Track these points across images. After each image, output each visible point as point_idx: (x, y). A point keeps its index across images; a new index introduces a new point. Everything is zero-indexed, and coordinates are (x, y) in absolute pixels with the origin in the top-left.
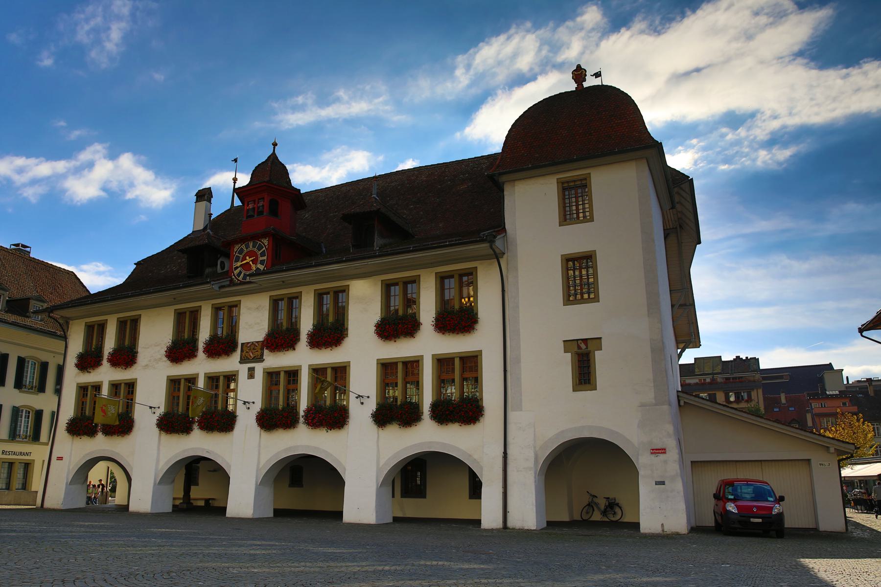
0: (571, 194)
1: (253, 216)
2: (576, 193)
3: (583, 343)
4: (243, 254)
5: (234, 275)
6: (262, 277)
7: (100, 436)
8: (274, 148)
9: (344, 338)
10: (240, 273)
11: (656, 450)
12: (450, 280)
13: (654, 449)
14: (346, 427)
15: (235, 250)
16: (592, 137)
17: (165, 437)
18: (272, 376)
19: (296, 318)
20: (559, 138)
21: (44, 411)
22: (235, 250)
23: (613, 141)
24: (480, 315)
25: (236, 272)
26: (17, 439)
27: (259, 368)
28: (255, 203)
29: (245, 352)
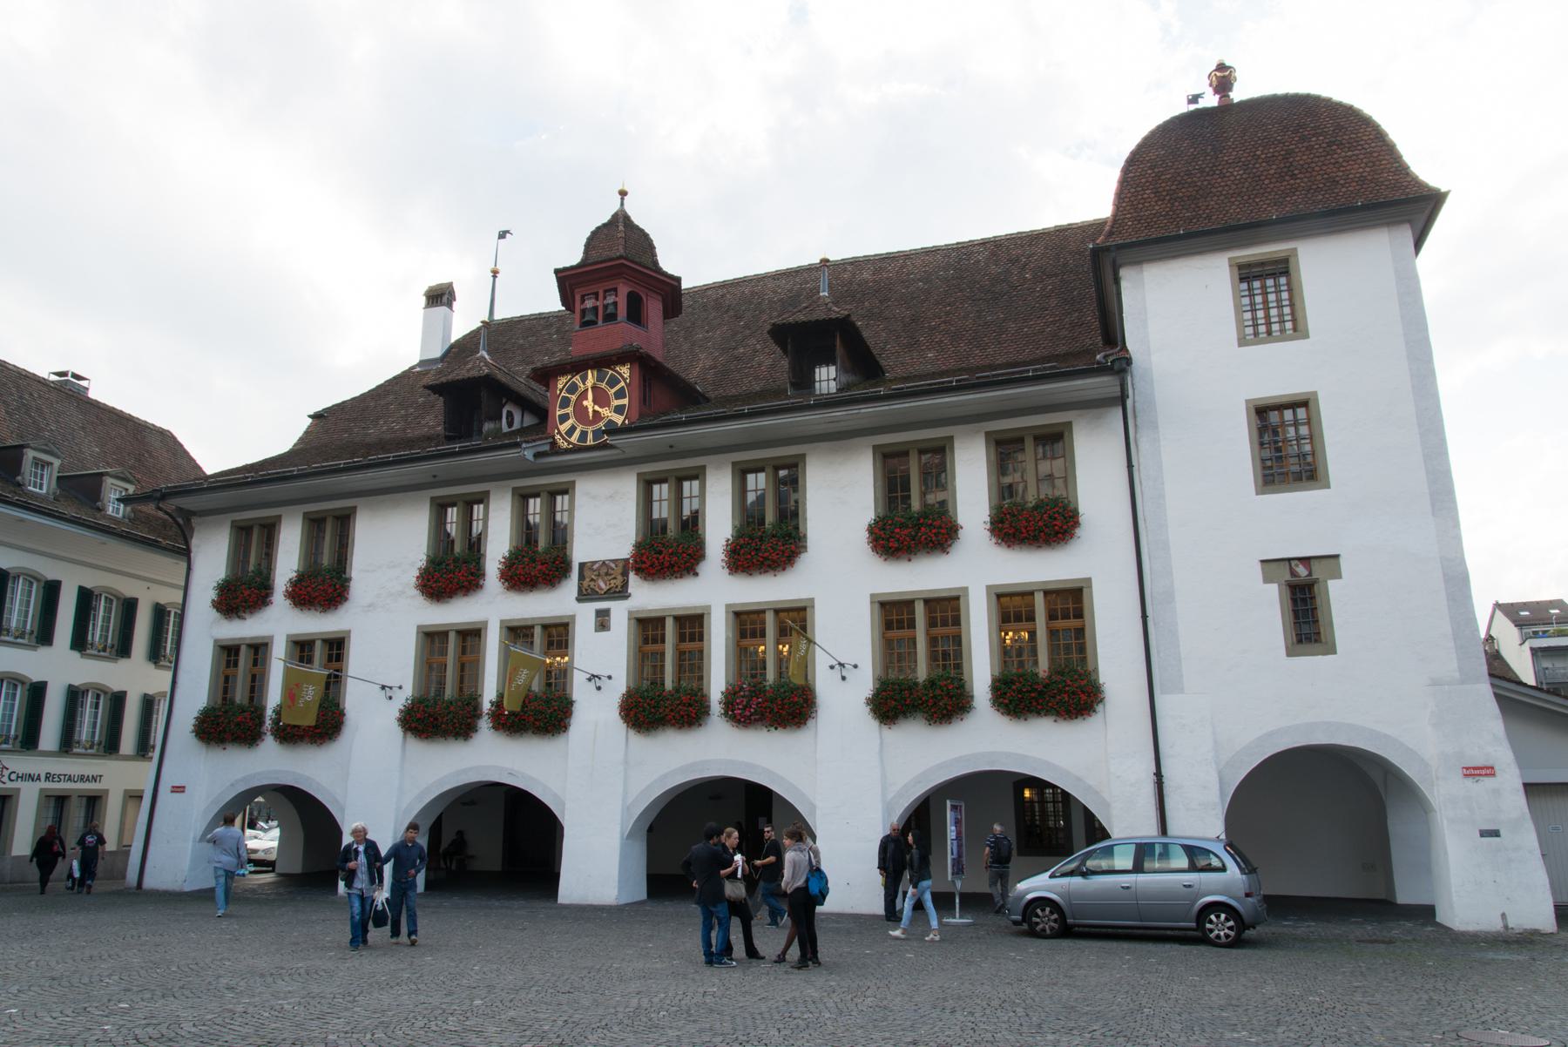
0: (1253, 289)
1: (593, 323)
2: (1264, 287)
3: (1300, 566)
4: (578, 394)
5: (559, 433)
6: (633, 436)
7: (269, 743)
8: (622, 199)
9: (800, 553)
10: (572, 430)
11: (1475, 768)
12: (756, 477)
13: (1470, 768)
14: (810, 723)
15: (560, 386)
16: (1298, 181)
17: (417, 747)
18: (648, 628)
19: (796, 502)
20: (1235, 187)
21: (128, 693)
22: (560, 386)
23: (1344, 190)
24: (1081, 510)
25: (564, 427)
26: (75, 750)
27: (619, 612)
28: (597, 299)
29: (588, 580)
